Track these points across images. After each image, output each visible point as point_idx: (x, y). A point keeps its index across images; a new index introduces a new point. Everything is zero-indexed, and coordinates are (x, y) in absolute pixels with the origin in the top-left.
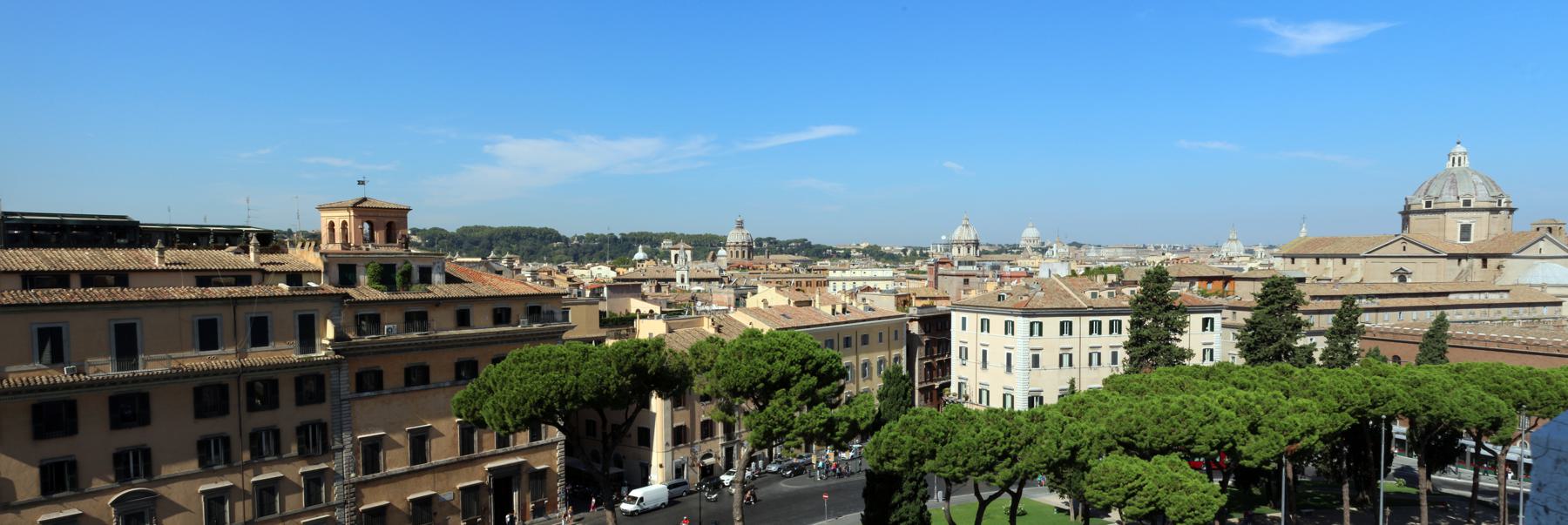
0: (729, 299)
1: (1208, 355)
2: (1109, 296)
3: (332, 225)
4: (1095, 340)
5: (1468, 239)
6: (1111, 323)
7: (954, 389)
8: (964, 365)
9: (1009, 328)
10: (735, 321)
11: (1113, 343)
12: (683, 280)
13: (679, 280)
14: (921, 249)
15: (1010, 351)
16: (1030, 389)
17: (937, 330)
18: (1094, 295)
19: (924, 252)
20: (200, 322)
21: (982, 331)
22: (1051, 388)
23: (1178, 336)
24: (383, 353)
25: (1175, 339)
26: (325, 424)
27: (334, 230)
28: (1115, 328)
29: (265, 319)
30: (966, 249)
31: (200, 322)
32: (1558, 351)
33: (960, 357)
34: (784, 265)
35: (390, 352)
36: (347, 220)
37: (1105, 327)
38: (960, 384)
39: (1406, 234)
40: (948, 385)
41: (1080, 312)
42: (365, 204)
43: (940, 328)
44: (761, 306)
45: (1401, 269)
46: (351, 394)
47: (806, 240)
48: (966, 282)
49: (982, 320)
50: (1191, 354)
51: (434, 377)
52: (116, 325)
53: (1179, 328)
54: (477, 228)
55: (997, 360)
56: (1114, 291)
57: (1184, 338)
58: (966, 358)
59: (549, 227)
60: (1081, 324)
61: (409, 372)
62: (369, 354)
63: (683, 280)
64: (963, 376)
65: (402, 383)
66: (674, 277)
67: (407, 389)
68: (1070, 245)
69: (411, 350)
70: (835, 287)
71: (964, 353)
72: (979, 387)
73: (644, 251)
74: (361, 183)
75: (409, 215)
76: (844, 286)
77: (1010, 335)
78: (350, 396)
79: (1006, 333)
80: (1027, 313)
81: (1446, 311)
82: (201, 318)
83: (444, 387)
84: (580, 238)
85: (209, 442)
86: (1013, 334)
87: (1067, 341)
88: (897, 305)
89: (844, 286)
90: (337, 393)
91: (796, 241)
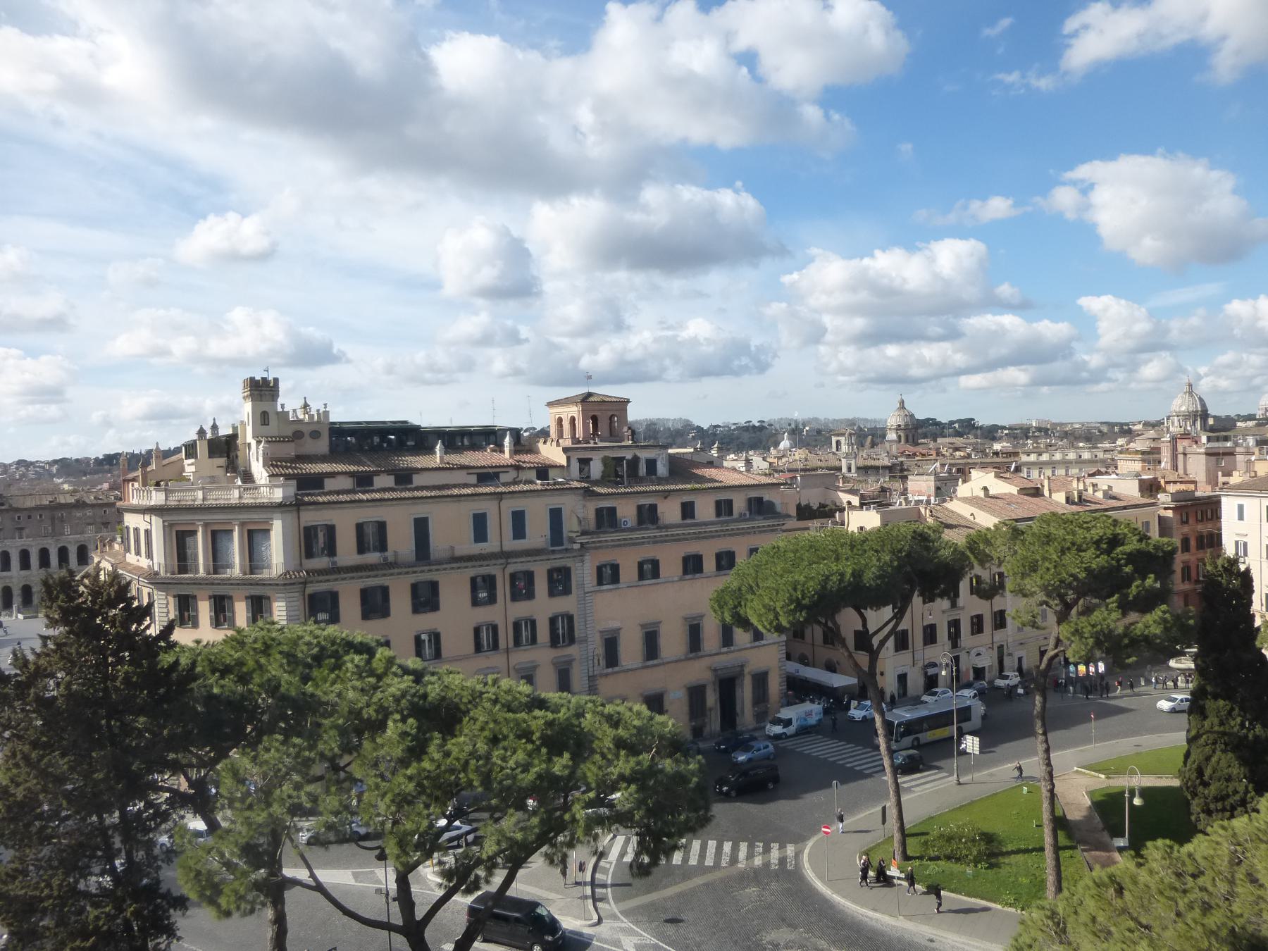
0: (929, 487)
3: (560, 421)
10: (952, 511)
12: (849, 469)
13: (844, 470)
14: (1121, 425)
19: (1126, 428)
24: (620, 546)
27: (574, 425)
30: (439, 543)
34: (957, 449)
35: (625, 545)
39: (553, 433)
42: (592, 399)
43: (1210, 516)
44: (982, 494)
47: (973, 419)
62: (607, 547)
63: (849, 469)
67: (641, 583)
68: (681, 921)
69: (643, 543)
75: (629, 406)
78: (592, 589)
88: (1141, 490)
90: (582, 586)
91: (959, 421)
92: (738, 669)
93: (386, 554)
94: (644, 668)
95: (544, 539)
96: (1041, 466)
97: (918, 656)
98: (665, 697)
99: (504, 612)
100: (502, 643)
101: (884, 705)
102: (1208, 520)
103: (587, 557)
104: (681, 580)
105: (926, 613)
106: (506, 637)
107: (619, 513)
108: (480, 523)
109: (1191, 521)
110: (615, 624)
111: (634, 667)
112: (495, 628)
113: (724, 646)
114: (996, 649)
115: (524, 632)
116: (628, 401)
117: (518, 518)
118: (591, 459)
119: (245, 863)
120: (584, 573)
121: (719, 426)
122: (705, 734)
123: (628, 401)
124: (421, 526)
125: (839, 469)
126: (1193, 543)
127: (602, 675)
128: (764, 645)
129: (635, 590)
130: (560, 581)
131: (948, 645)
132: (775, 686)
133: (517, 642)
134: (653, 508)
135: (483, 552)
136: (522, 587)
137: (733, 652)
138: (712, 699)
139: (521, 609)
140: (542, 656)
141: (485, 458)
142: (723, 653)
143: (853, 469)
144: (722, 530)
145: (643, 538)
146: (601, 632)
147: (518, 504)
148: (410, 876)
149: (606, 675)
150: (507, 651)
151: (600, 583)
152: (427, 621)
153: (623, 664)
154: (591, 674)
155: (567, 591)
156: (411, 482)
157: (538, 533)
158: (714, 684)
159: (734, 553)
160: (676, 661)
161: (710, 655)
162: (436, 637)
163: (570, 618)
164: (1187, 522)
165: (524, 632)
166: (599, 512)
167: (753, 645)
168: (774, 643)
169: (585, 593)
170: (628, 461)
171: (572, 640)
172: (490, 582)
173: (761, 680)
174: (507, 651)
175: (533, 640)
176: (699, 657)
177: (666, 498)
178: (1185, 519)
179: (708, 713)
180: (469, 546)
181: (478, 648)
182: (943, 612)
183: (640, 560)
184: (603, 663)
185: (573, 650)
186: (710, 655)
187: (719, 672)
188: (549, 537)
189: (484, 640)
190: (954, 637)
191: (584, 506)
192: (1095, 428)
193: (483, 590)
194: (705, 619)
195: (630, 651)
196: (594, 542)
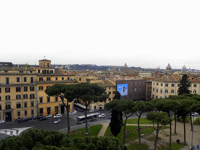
1: (195, 92)
2: (47, 80)
7: (152, 96)
9: (162, 85)
11: (176, 88)
41: (170, 82)
48: (161, 76)
50: (191, 92)
53: (189, 86)
54: (90, 65)
57: (190, 88)
65: (16, 108)
77: (167, 87)
80: (165, 82)
81: (170, 137)
84: (100, 66)
87: (173, 88)
90: (36, 90)
96: (141, 75)
100: (21, 98)
101: (100, 116)
103: (37, 85)
108: (18, 80)
115: (25, 97)
116: (51, 61)
120: (37, 88)
123: (51, 61)
124: (7, 79)
130: (32, 89)
133: (24, 98)
136: (26, 90)
138: (59, 109)
139: (25, 93)
140: (29, 101)
147: (25, 76)
151: (39, 89)
152: (8, 94)
157: (29, 80)
165: (25, 97)
181: (17, 98)
185: (34, 100)
189: (18, 97)
193: (18, 90)
194: (28, 103)
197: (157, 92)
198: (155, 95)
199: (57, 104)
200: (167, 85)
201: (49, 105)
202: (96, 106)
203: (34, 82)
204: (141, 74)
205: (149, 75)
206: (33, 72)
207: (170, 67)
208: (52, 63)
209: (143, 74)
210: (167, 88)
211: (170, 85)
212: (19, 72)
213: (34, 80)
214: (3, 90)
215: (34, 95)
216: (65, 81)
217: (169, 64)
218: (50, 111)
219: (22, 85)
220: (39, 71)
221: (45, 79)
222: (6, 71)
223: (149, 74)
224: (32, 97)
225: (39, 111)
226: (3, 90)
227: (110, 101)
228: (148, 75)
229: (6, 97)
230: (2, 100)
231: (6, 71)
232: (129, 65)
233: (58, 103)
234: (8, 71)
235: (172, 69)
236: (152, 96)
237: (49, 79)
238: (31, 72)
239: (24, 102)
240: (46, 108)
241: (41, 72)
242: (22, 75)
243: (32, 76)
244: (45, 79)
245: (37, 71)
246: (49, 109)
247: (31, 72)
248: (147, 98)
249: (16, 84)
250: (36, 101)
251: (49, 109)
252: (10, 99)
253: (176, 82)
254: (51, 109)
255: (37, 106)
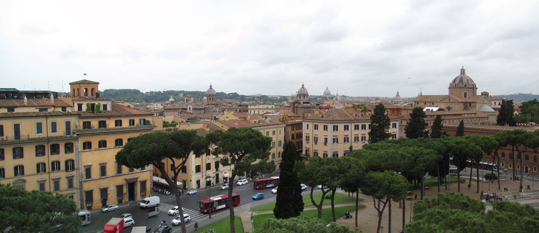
4: (357, 132)
5: (466, 97)
6: (362, 125)
7: (304, 153)
8: (308, 143)
9: (326, 128)
12: (190, 109)
13: (188, 109)
15: (326, 137)
16: (334, 151)
17: (297, 129)
18: (356, 115)
20: (15, 125)
21: (315, 129)
22: (341, 149)
23: (387, 130)
25: (386, 131)
26: (74, 160)
28: (364, 127)
29: (56, 123)
31: (15, 125)
32: (489, 132)
33: (306, 139)
36: (79, 88)
37: (360, 127)
38: (306, 151)
40: (302, 151)
41: (351, 121)
45: (449, 106)
46: (81, 150)
47: (237, 93)
49: (315, 125)
51: (109, 145)
52: (14, 124)
54: (111, 90)
55: (321, 140)
56: (363, 114)
58: (309, 140)
59: (136, 89)
60: (352, 127)
61: (100, 142)
63: (190, 109)
64: (308, 147)
66: (186, 108)
67: (99, 149)
70: (251, 112)
71: (308, 138)
72: (314, 151)
73: (173, 98)
74: (85, 74)
76: (254, 112)
79: (324, 130)
80: (331, 122)
82: (37, 122)
83: (112, 148)
85: (55, 163)
86: (327, 130)
89: (254, 112)
90: (77, 149)
91: (232, 94)
92: (135, 180)
93: (3, 137)
94: (100, 179)
95: (63, 132)
97: (204, 174)
98: (108, 189)
99: (48, 158)
102: (300, 129)
103: (80, 139)
104: (114, 148)
105: (207, 159)
106: (48, 167)
107: (92, 124)
109: (295, 129)
110: (90, 164)
111: (97, 178)
112: (45, 164)
113: (118, 174)
114: (231, 171)
115: (56, 166)
116: (98, 83)
117: (54, 125)
118: (82, 104)
119: (511, 137)
120: (79, 145)
121: (148, 93)
122: (123, 202)
123: (98, 83)
124: (17, 128)
125: (187, 109)
126: (295, 136)
127: (84, 181)
128: (145, 171)
129: (98, 151)
130: (69, 148)
131: (215, 171)
132: (149, 186)
134: (104, 122)
135: (41, 137)
136: (55, 149)
137: (133, 174)
138: (125, 190)
140: (62, 175)
141: (43, 101)
142: (130, 174)
143: (191, 109)
144: (130, 131)
145: (100, 133)
146: (84, 166)
148: (134, 228)
149: (86, 181)
150: (49, 173)
152: (19, 162)
153: (93, 177)
154: (80, 181)
155: (72, 151)
156: (14, 111)
157: (61, 131)
158: (126, 185)
159: (122, 140)
160: (112, 177)
161: (125, 175)
162: (22, 167)
163: (73, 161)
164: (293, 130)
165: (56, 166)
166: (84, 123)
167: (141, 171)
168: (148, 171)
169: (79, 152)
170: (96, 105)
171: (73, 169)
172: (43, 147)
173: (143, 183)
174: (49, 173)
175: (59, 169)
176: (120, 175)
177: (109, 119)
178: (293, 129)
179: (124, 195)
180: (34, 135)
181: (38, 171)
182: (213, 159)
183: (100, 141)
184: (85, 177)
185: (74, 173)
186: (125, 175)
187: (128, 181)
188: (65, 132)
189: (41, 168)
190: (217, 167)
191: (79, 121)
192: (276, 97)
193: (40, 151)
195: (96, 172)
196: (82, 134)
197: (316, 143)
198: (311, 150)
199: (120, 180)
200: (336, 128)
201: (104, 184)
202: (199, 181)
203: (74, 133)
204: (253, 107)
205: (270, 109)
206: (69, 110)
207: (306, 93)
208: (101, 88)
209: (257, 107)
210: (336, 133)
211: (341, 127)
212: (38, 111)
213: (72, 128)
214: (8, 153)
215: (73, 161)
216: (124, 128)
217: (303, 85)
218: (107, 196)
219: (48, 139)
220: (80, 106)
221: (95, 123)
222: (11, 109)
223: (270, 107)
224: (70, 165)
225: (84, 198)
226: (8, 153)
227: (171, 179)
228: (267, 108)
229: (38, 165)
230: (6, 176)
231: (11, 109)
232: (217, 90)
233: (123, 177)
234: (48, 109)
235: (309, 95)
236: (304, 153)
237: (102, 124)
238: (64, 108)
239: (53, 179)
240: (99, 191)
241: (84, 108)
242: (46, 117)
243: (68, 119)
244: (95, 123)
245: (76, 108)
246: (104, 192)
247: (64, 108)
248: (27, 204)
249: (35, 139)
250: (78, 174)
251: (104, 192)
252: (23, 173)
253: (366, 121)
254: (109, 192)
255: (81, 187)
